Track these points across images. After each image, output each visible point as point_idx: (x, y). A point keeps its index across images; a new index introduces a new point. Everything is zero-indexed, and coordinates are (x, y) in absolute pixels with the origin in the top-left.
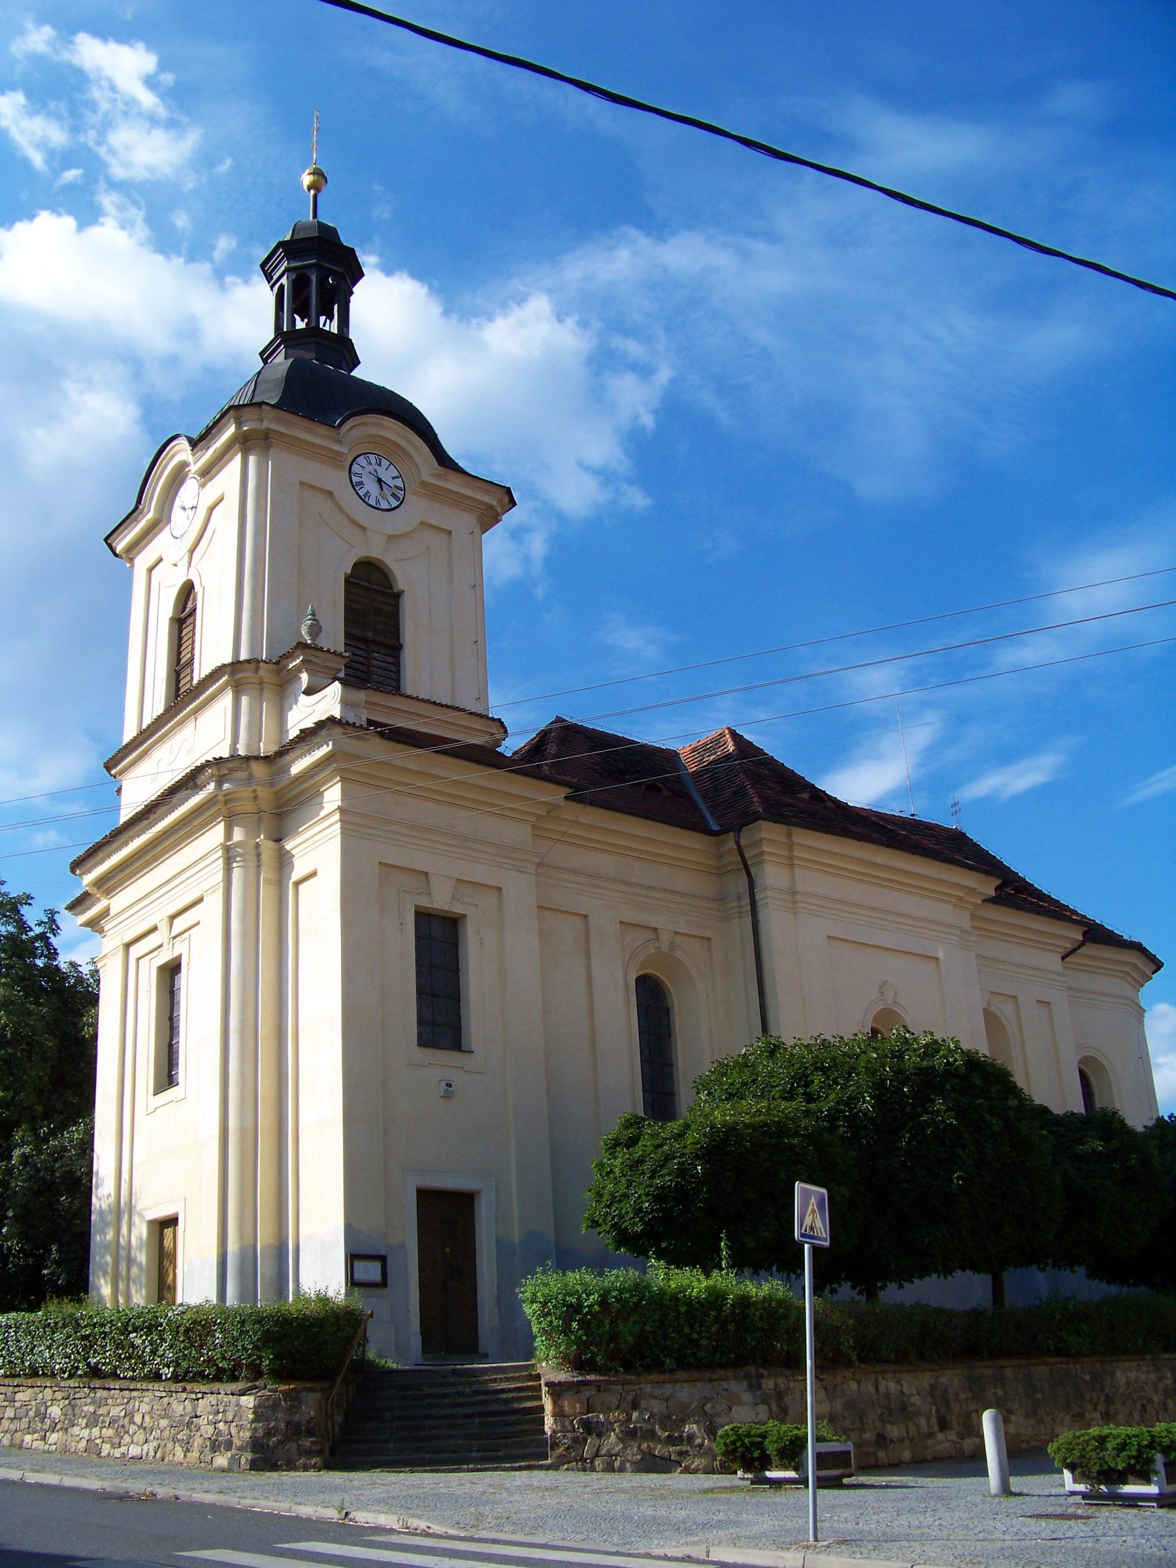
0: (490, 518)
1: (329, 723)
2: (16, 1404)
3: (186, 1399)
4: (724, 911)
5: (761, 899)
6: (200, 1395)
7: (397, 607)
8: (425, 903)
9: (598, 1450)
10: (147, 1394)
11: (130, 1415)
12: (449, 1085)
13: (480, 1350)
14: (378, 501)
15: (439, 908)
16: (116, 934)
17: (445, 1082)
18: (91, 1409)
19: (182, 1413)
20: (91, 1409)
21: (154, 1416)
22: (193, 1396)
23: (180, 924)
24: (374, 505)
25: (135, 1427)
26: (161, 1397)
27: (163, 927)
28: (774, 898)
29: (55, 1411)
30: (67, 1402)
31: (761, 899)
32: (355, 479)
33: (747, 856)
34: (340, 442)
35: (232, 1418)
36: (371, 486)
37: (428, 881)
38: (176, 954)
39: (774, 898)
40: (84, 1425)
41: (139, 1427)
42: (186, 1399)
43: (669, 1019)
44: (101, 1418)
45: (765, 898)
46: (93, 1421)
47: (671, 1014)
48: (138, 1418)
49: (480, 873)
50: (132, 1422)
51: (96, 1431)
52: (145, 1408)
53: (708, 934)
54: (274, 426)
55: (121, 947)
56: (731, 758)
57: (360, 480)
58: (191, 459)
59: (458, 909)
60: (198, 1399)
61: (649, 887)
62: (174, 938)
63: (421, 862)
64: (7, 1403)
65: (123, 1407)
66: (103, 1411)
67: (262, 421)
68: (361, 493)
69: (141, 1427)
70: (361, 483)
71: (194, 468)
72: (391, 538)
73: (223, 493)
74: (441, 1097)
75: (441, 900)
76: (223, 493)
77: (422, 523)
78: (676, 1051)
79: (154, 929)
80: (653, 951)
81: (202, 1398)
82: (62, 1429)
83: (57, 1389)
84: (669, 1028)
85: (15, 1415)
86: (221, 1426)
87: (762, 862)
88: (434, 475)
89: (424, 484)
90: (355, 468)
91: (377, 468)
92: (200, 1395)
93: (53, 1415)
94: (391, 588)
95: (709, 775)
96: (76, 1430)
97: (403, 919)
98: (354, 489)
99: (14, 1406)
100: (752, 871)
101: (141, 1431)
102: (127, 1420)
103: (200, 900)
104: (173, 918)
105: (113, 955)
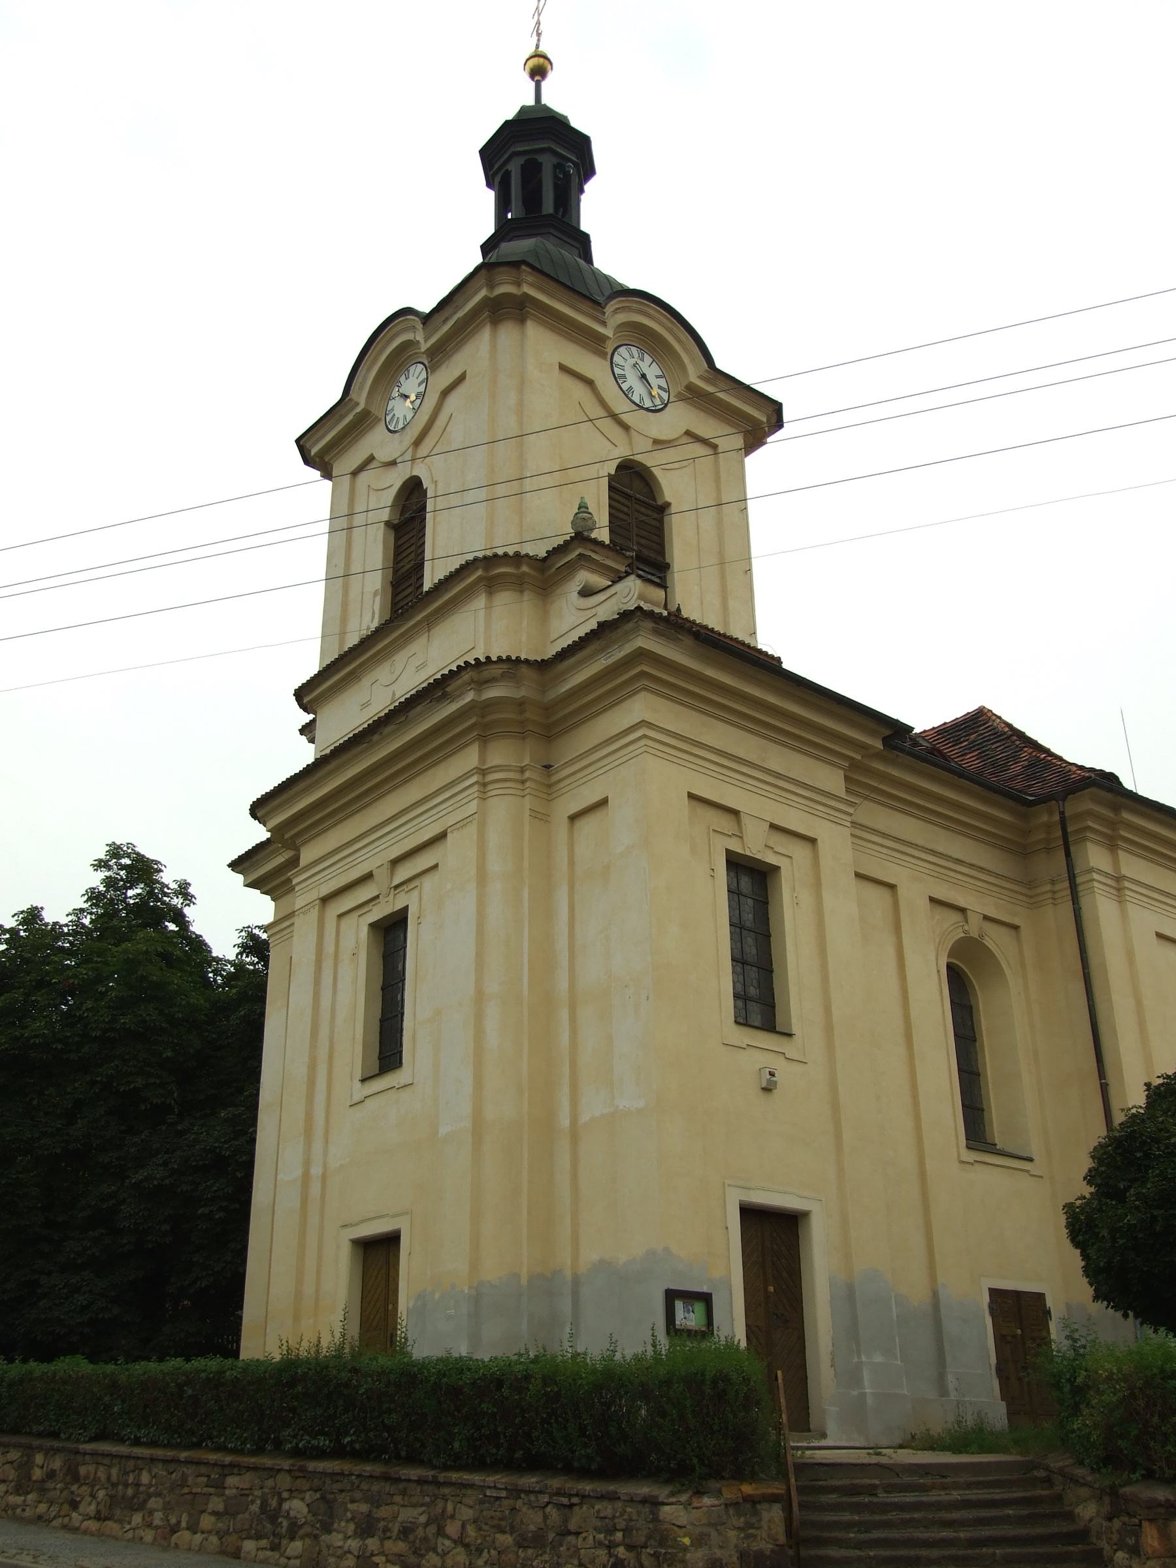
0: (755, 438)
1: (639, 614)
2: (227, 1492)
3: (548, 1503)
4: (1031, 897)
5: (1084, 883)
6: (575, 1500)
7: (661, 521)
8: (736, 847)
9: (628, 1501)
10: (469, 1492)
11: (438, 1522)
12: (772, 1074)
13: (811, 1427)
14: (642, 399)
15: (751, 855)
16: (311, 887)
17: (768, 1070)
18: (364, 1508)
19: (542, 1526)
20: (364, 1508)
21: (485, 1527)
22: (565, 1501)
23: (403, 873)
24: (638, 402)
25: (447, 1543)
26: (498, 1498)
27: (381, 876)
28: (1099, 882)
29: (297, 1507)
30: (318, 1495)
31: (1084, 883)
32: (617, 371)
33: (1070, 829)
34: (604, 324)
35: (643, 1539)
36: (632, 381)
37: (739, 821)
38: (399, 906)
39: (1099, 882)
40: (350, 1533)
41: (455, 1542)
42: (548, 1503)
43: (972, 1021)
44: (382, 1524)
45: (1088, 881)
46: (366, 1528)
47: (974, 1014)
48: (452, 1529)
49: (795, 820)
50: (441, 1532)
51: (372, 1543)
52: (467, 1513)
53: (1016, 922)
54: (532, 292)
55: (318, 901)
56: (1000, 736)
57: (622, 372)
58: (420, 337)
59: (771, 859)
60: (571, 1506)
61: (957, 859)
62: (396, 887)
63: (731, 797)
64: (211, 1490)
65: (424, 1508)
66: (383, 1512)
67: (519, 285)
68: (625, 387)
69: (460, 1541)
70: (624, 376)
71: (424, 347)
72: (656, 442)
73: (465, 371)
74: (763, 1089)
75: (755, 846)
76: (465, 371)
77: (688, 433)
78: (984, 1057)
79: (368, 877)
80: (963, 935)
81: (581, 1504)
82: (308, 1535)
83: (301, 1474)
84: (973, 1029)
85: (226, 1507)
86: (621, 1551)
87: (1085, 839)
88: (701, 377)
89: (690, 388)
90: (617, 359)
91: (639, 362)
92: (575, 1500)
93: (292, 1514)
94: (654, 499)
95: (976, 753)
96: (336, 1539)
97: (714, 865)
98: (617, 382)
99: (223, 1495)
100: (1072, 849)
101: (460, 1549)
102: (432, 1529)
103: (443, 836)
104: (395, 862)
105: (304, 913)
